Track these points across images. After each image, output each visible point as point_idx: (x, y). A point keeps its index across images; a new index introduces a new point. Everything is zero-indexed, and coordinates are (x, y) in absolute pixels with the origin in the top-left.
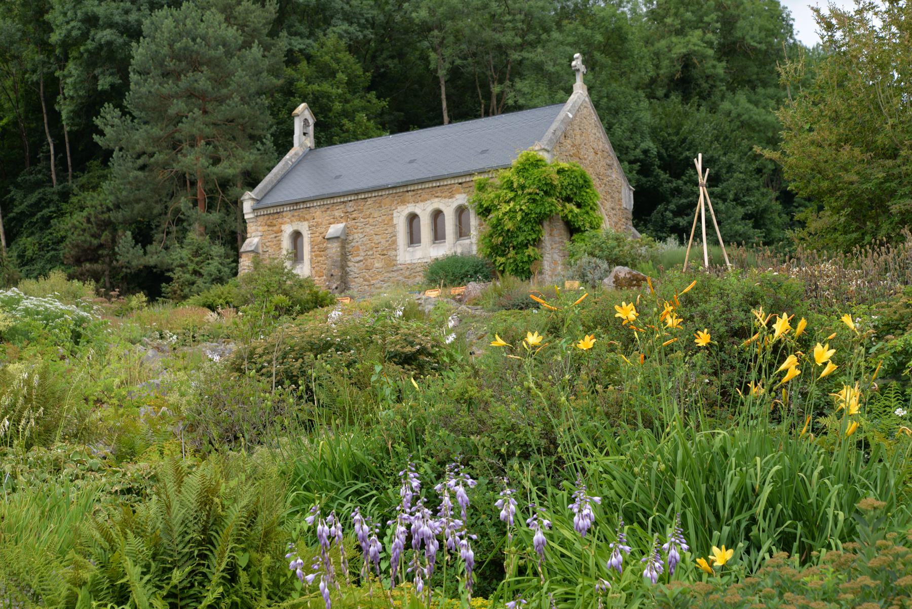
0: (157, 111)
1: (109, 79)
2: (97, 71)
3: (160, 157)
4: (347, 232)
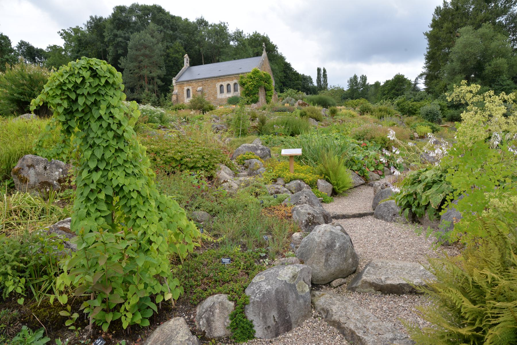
0: (135, 59)
1: (121, 51)
2: (118, 49)
3: (136, 71)
4: (203, 89)
